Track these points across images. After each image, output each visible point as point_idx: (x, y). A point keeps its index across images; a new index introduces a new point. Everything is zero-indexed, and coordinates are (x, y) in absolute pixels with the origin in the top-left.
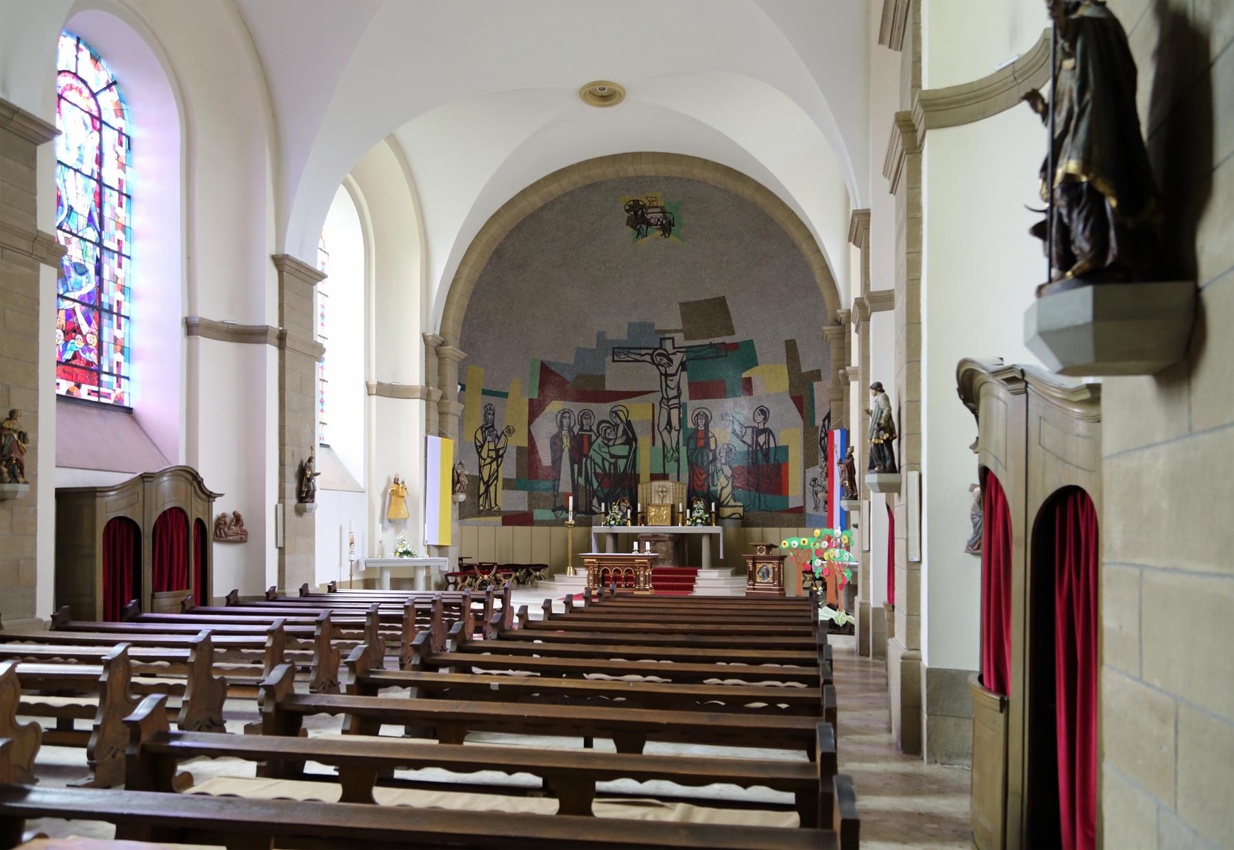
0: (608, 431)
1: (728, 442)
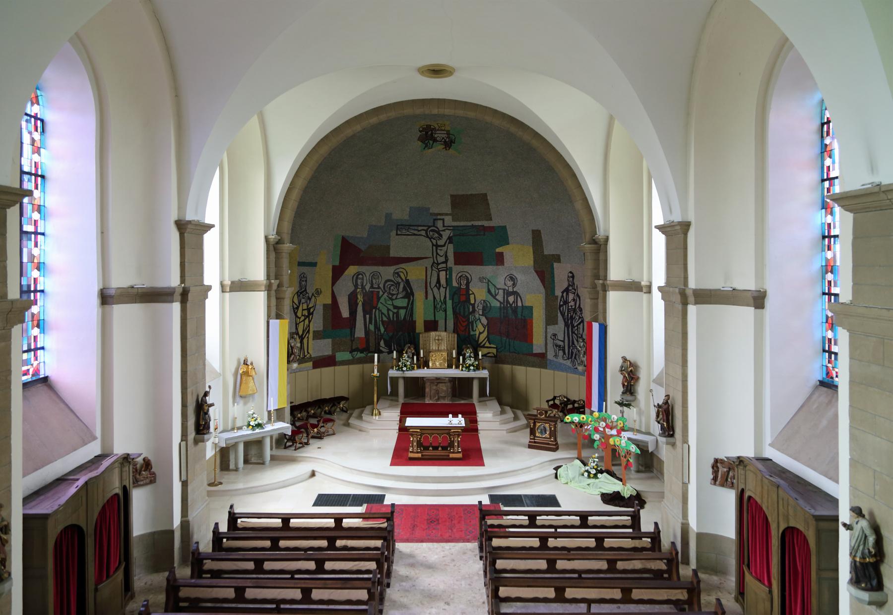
0: (392, 288)
1: (484, 299)
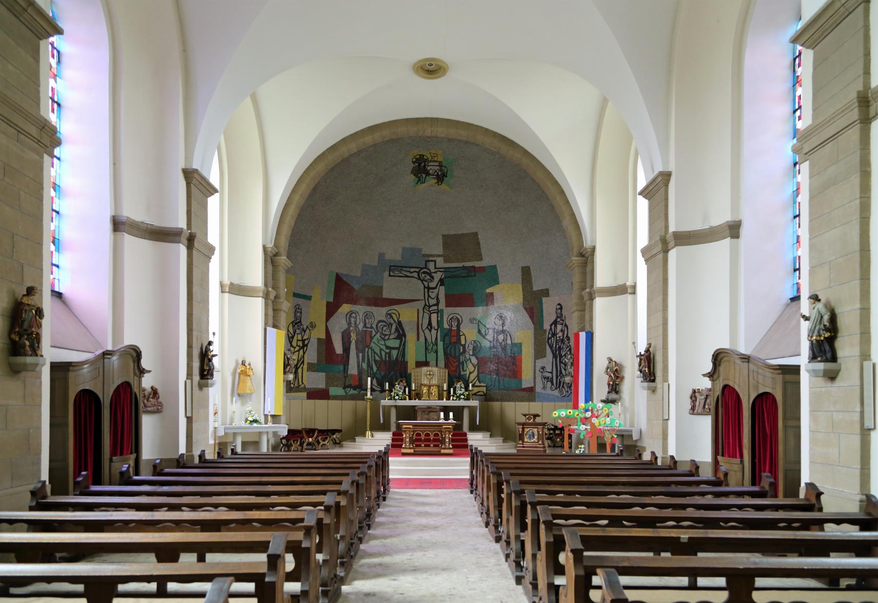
0: (385, 328)
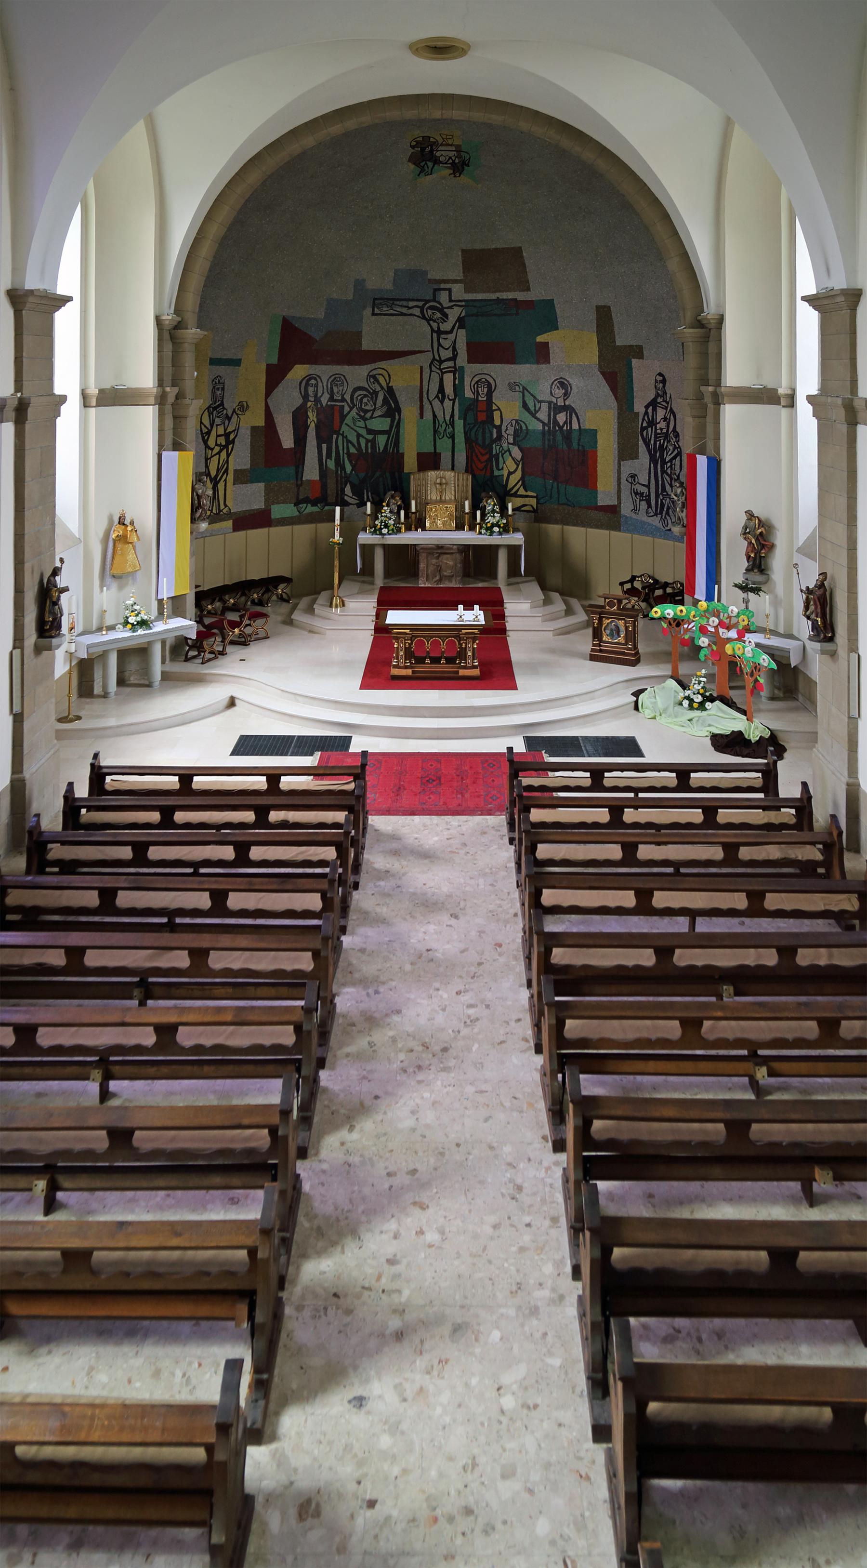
0: (365, 400)
1: (517, 418)
